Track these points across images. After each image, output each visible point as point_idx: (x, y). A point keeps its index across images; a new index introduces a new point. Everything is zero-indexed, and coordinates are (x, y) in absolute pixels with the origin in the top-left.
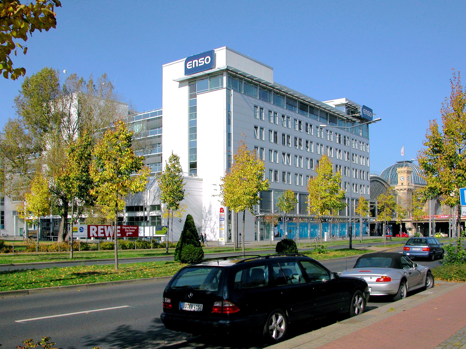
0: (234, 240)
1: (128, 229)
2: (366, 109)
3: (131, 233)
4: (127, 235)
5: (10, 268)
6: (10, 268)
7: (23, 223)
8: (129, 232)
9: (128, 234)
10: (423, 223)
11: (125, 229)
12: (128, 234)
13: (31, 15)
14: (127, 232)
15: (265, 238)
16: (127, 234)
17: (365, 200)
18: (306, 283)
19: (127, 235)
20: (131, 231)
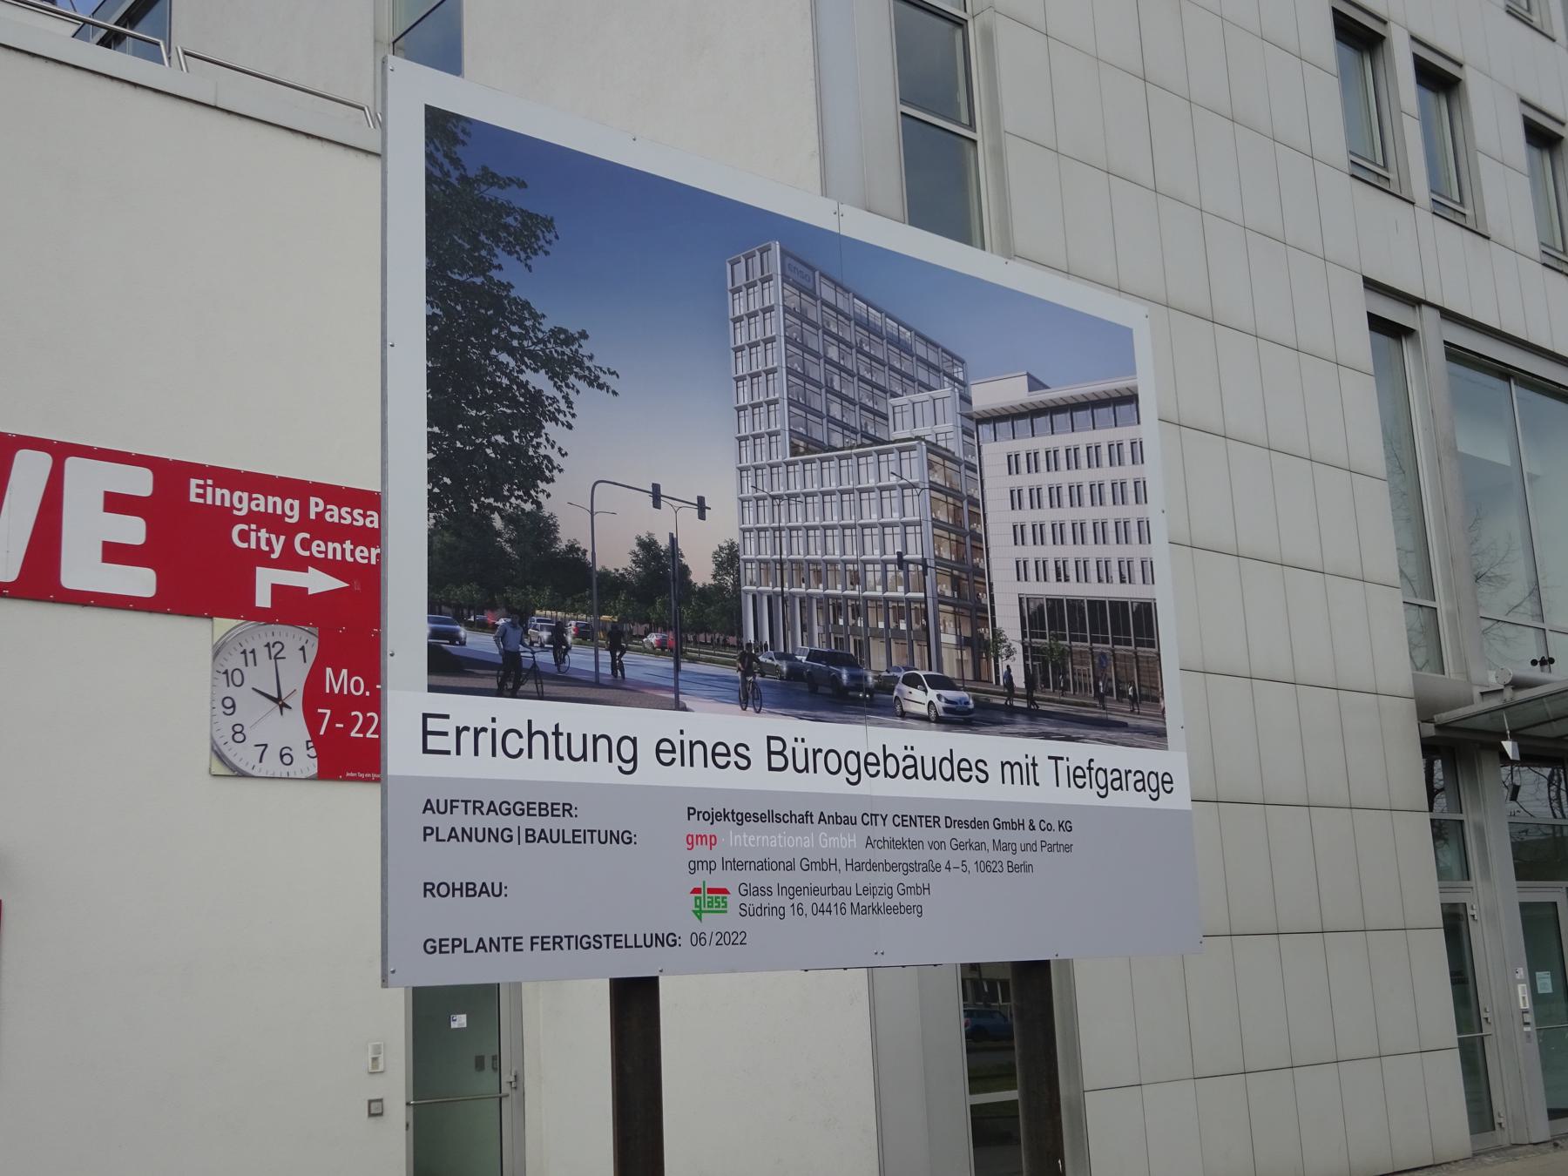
0: (804, 549)
1: (274, 523)
2: (551, 610)
3: (317, 582)
4: (263, 599)
5: (1507, 615)
6: (1507, 615)
7: (161, 66)
8: (290, 561)
9: (277, 590)
10: (1545, 982)
11: (226, 516)
12: (277, 590)
13: (933, 565)
14: (264, 559)
15: (697, 844)
16: (266, 580)
17: (1021, 639)
18: (951, 525)
19: (263, 599)
20: (334, 550)
